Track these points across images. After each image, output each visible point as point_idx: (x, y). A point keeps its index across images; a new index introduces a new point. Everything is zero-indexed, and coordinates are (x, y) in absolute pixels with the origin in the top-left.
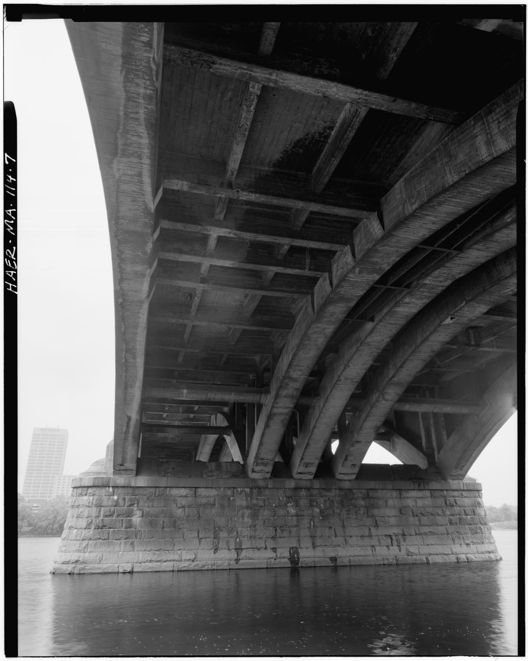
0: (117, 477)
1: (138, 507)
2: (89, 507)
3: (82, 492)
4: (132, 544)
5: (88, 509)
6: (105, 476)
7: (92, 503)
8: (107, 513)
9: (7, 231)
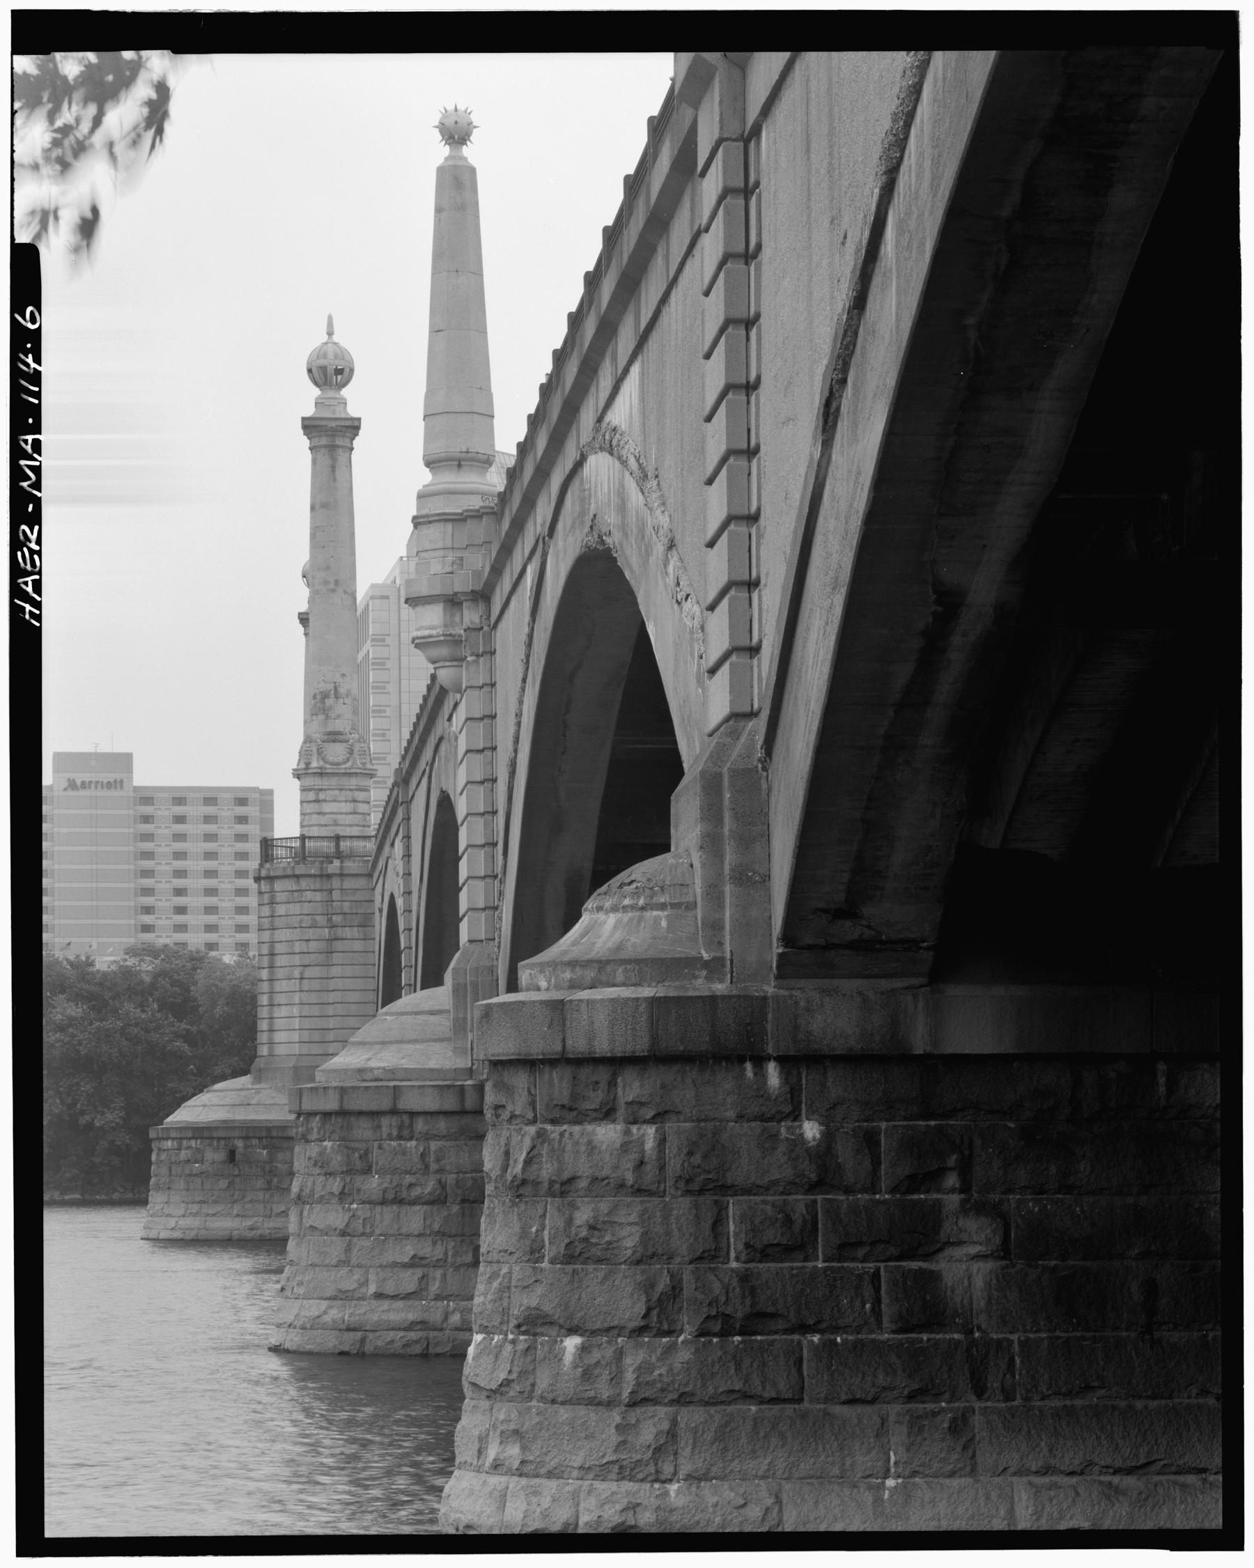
0: (805, 991)
1: (965, 1188)
2: (639, 1191)
3: (574, 1096)
4: (958, 1426)
5: (637, 1204)
6: (720, 988)
7: (662, 1168)
8: (772, 1235)
9: (22, 487)
